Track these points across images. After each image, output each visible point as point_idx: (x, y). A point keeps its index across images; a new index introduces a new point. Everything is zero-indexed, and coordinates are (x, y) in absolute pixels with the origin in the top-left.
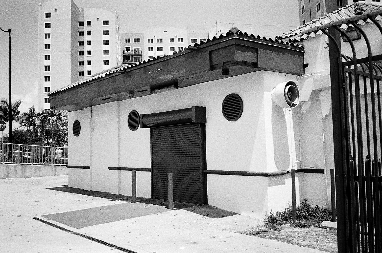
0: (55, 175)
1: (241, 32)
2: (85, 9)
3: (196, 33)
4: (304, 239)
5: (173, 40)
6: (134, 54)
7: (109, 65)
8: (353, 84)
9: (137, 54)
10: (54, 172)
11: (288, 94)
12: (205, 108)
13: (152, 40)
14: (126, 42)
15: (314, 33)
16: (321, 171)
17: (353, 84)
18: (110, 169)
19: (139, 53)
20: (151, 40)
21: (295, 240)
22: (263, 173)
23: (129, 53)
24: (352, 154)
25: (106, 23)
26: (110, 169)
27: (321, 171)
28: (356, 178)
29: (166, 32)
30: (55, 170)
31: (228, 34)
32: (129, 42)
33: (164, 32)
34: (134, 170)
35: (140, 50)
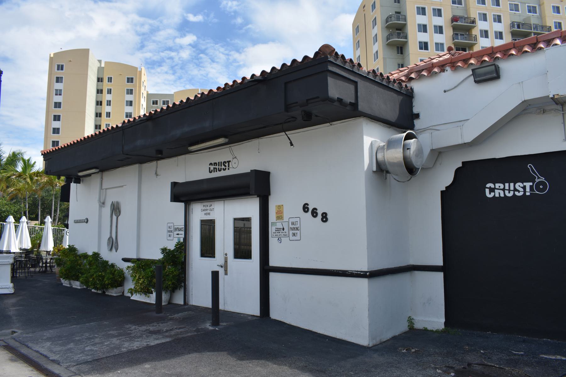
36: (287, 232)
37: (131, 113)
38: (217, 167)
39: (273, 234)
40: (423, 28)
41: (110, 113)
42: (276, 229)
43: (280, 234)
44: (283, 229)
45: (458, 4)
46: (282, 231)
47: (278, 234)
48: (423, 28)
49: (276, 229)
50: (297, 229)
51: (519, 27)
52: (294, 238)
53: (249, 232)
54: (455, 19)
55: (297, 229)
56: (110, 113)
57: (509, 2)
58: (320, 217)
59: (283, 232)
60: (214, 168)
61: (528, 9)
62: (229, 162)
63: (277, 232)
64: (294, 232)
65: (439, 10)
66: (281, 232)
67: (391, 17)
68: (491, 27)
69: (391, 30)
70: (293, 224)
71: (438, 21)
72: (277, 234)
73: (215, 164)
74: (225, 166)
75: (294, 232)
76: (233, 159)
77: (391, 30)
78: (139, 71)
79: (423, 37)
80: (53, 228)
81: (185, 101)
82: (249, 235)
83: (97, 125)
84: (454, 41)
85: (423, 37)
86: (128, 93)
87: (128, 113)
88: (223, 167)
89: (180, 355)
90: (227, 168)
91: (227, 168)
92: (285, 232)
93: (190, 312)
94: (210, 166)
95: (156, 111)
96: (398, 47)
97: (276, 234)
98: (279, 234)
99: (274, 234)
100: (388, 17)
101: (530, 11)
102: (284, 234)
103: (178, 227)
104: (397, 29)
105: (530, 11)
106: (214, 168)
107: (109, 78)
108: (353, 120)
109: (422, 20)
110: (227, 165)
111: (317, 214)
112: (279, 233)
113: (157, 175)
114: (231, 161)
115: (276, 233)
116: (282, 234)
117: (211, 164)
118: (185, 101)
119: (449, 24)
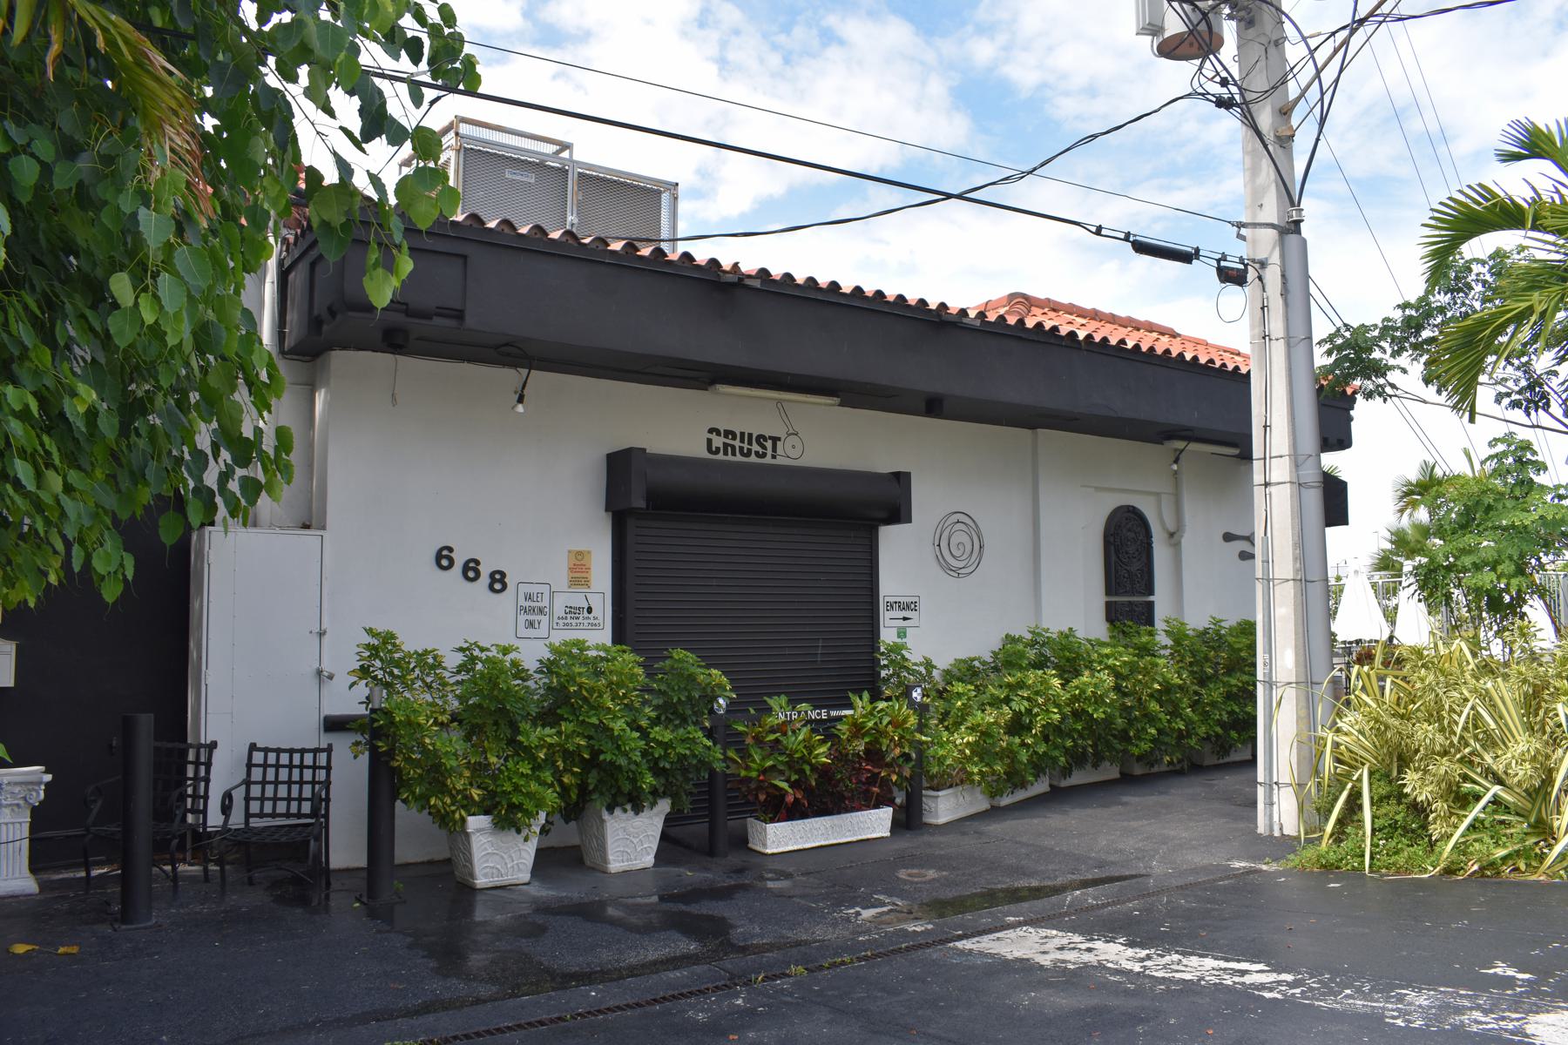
36: (601, 618)
38: (737, 443)
39: (556, 620)
42: (568, 610)
43: (580, 620)
44: (590, 610)
46: (586, 614)
47: (574, 622)
49: (568, 610)
50: (541, 611)
52: (531, 632)
55: (541, 611)
58: (485, 579)
59: (589, 618)
60: (724, 443)
62: (775, 440)
63: (569, 616)
64: (531, 617)
66: (581, 616)
70: (529, 597)
72: (569, 621)
73: (728, 433)
74: (764, 447)
75: (531, 617)
76: (789, 435)
80: (1151, 598)
81: (1174, 354)
88: (755, 447)
90: (769, 452)
91: (769, 452)
92: (595, 618)
94: (710, 436)
95: (1167, 351)
97: (566, 621)
98: (578, 621)
99: (561, 622)
102: (592, 621)
103: (898, 599)
106: (724, 443)
108: (826, 405)
110: (769, 444)
111: (451, 562)
112: (578, 618)
114: (783, 440)
115: (566, 618)
116: (586, 622)
117: (711, 431)
118: (1174, 354)
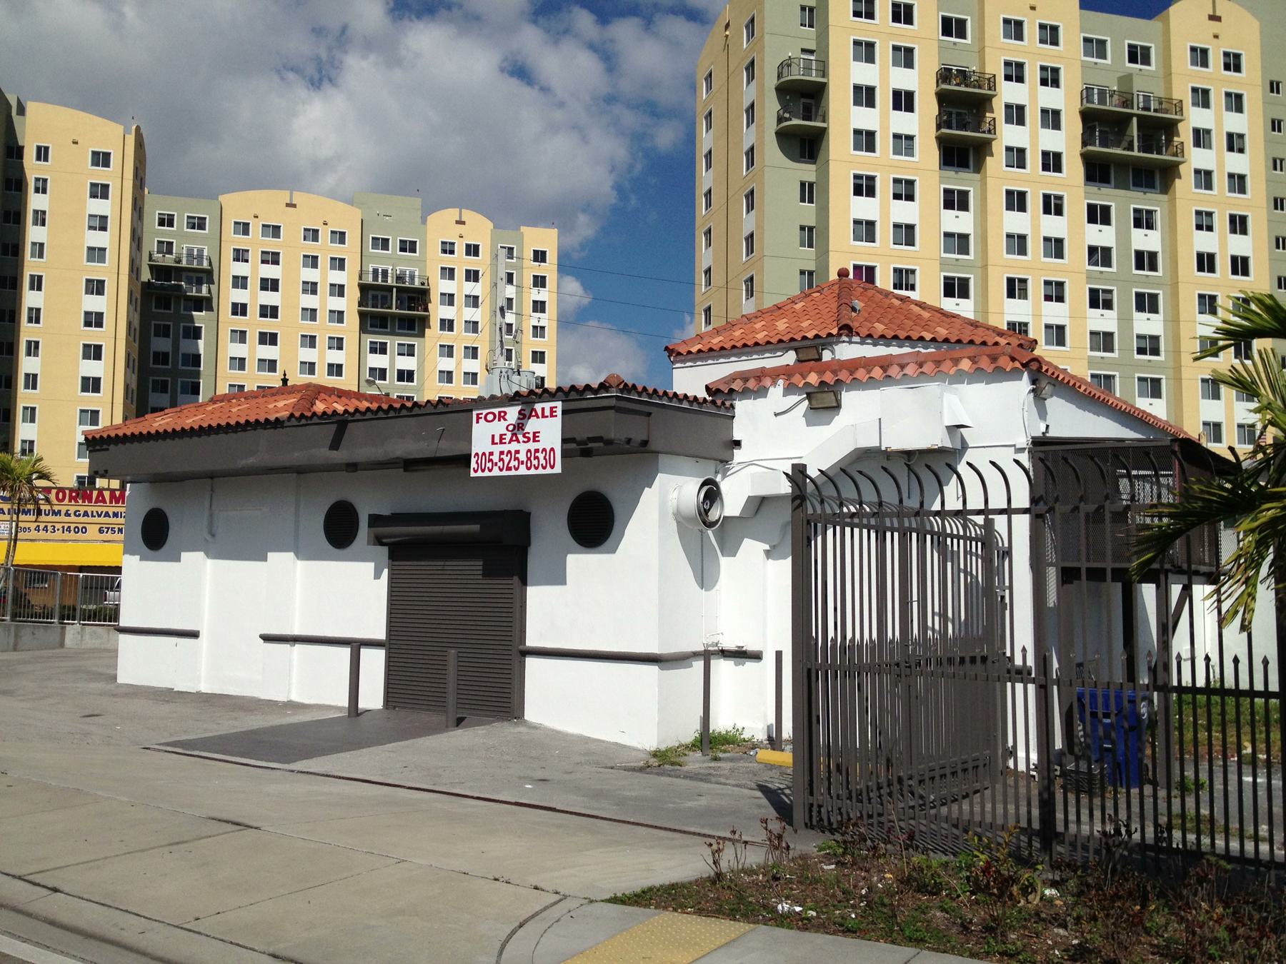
0: (15, 649)
1: (626, 385)
2: (31, 107)
3: (387, 218)
4: (727, 779)
5: (313, 234)
6: (184, 263)
7: (103, 295)
8: (819, 539)
9: (195, 265)
10: (12, 640)
11: (703, 503)
12: (530, 513)
13: (246, 225)
14: (162, 223)
15: (756, 380)
16: (757, 656)
17: (819, 539)
18: (267, 638)
19: (200, 263)
20: (244, 228)
21: (713, 779)
22: (309, 636)
23: (169, 260)
24: (814, 634)
25: (102, 159)
26: (267, 638)
27: (757, 656)
28: (949, 535)
29: (294, 206)
30: (16, 636)
31: (603, 386)
32: (171, 224)
33: (288, 205)
34: (356, 646)
35: (205, 253)
37: (102, 314)
40: (865, 96)
41: (35, 376)
45: (956, 37)
48: (865, 96)
51: (1102, 100)
53: (1167, 113)
54: (945, 75)
56: (35, 376)
57: (1083, 35)
61: (1129, 51)
65: (909, 51)
67: (789, 65)
68: (1033, 97)
69: (788, 97)
71: (904, 79)
77: (788, 97)
78: (130, 133)
79: (865, 118)
82: (800, 356)
83: (10, 213)
84: (939, 132)
85: (865, 118)
86: (93, 196)
87: (91, 313)
89: (910, 944)
93: (1273, 511)
96: (803, 142)
100: (782, 63)
101: (1133, 59)
104: (804, 95)
105: (1133, 59)
107: (39, 148)
109: (864, 74)
113: (315, 139)
119: (932, 88)
